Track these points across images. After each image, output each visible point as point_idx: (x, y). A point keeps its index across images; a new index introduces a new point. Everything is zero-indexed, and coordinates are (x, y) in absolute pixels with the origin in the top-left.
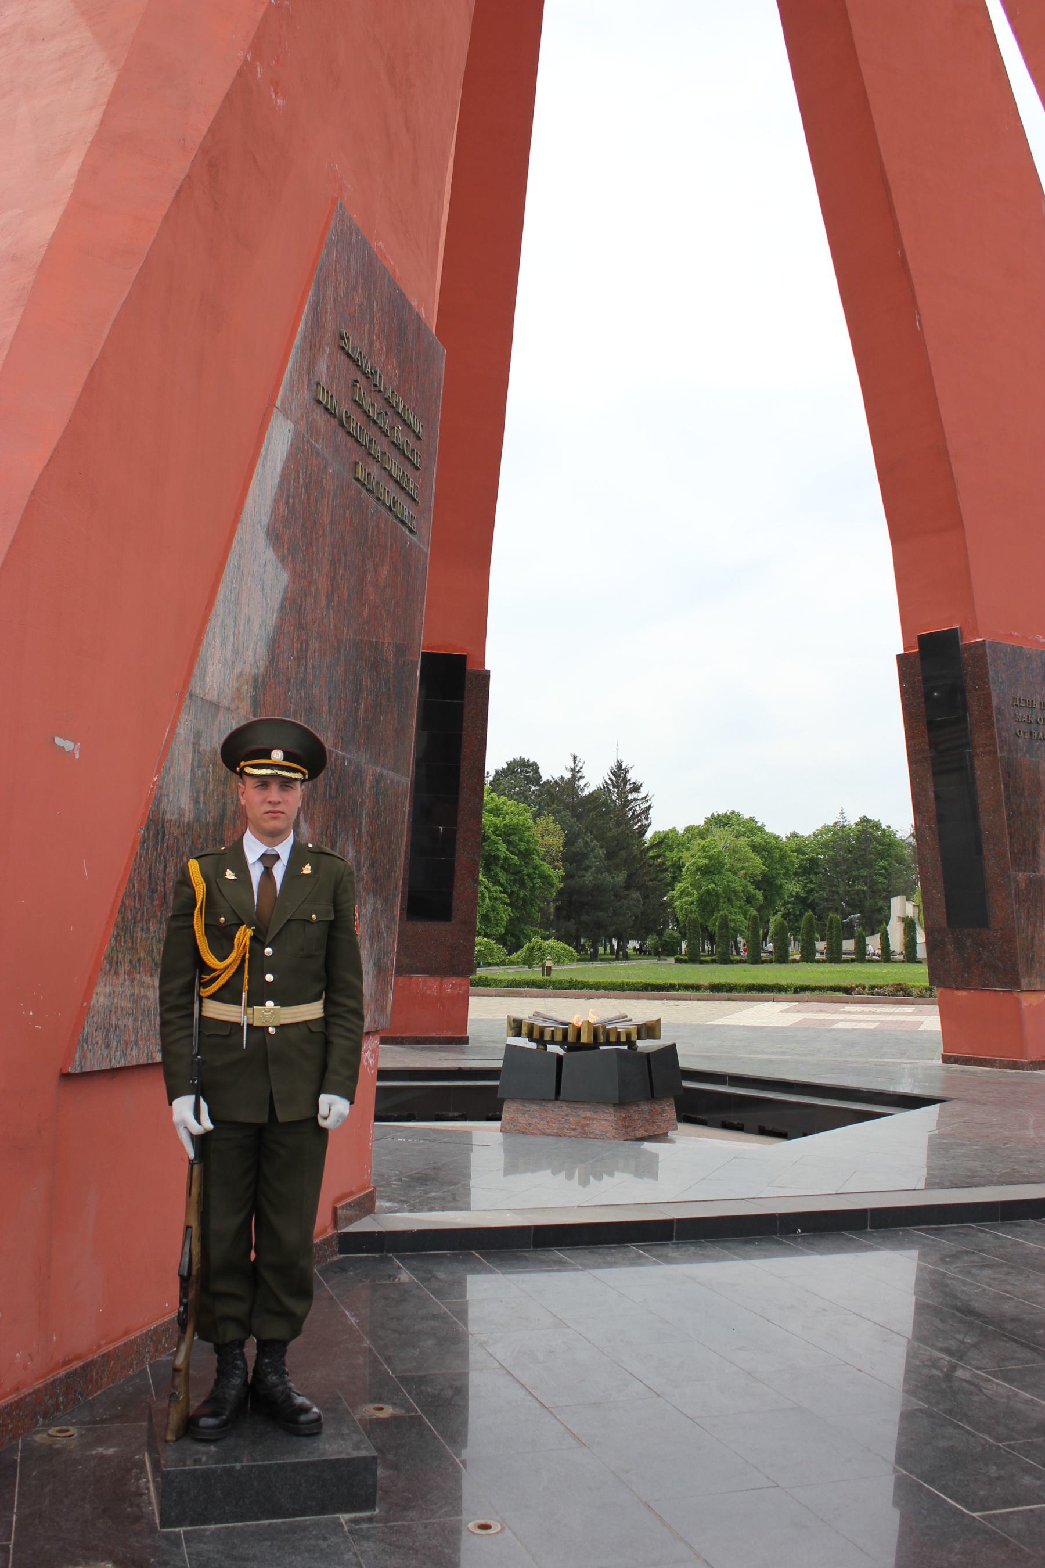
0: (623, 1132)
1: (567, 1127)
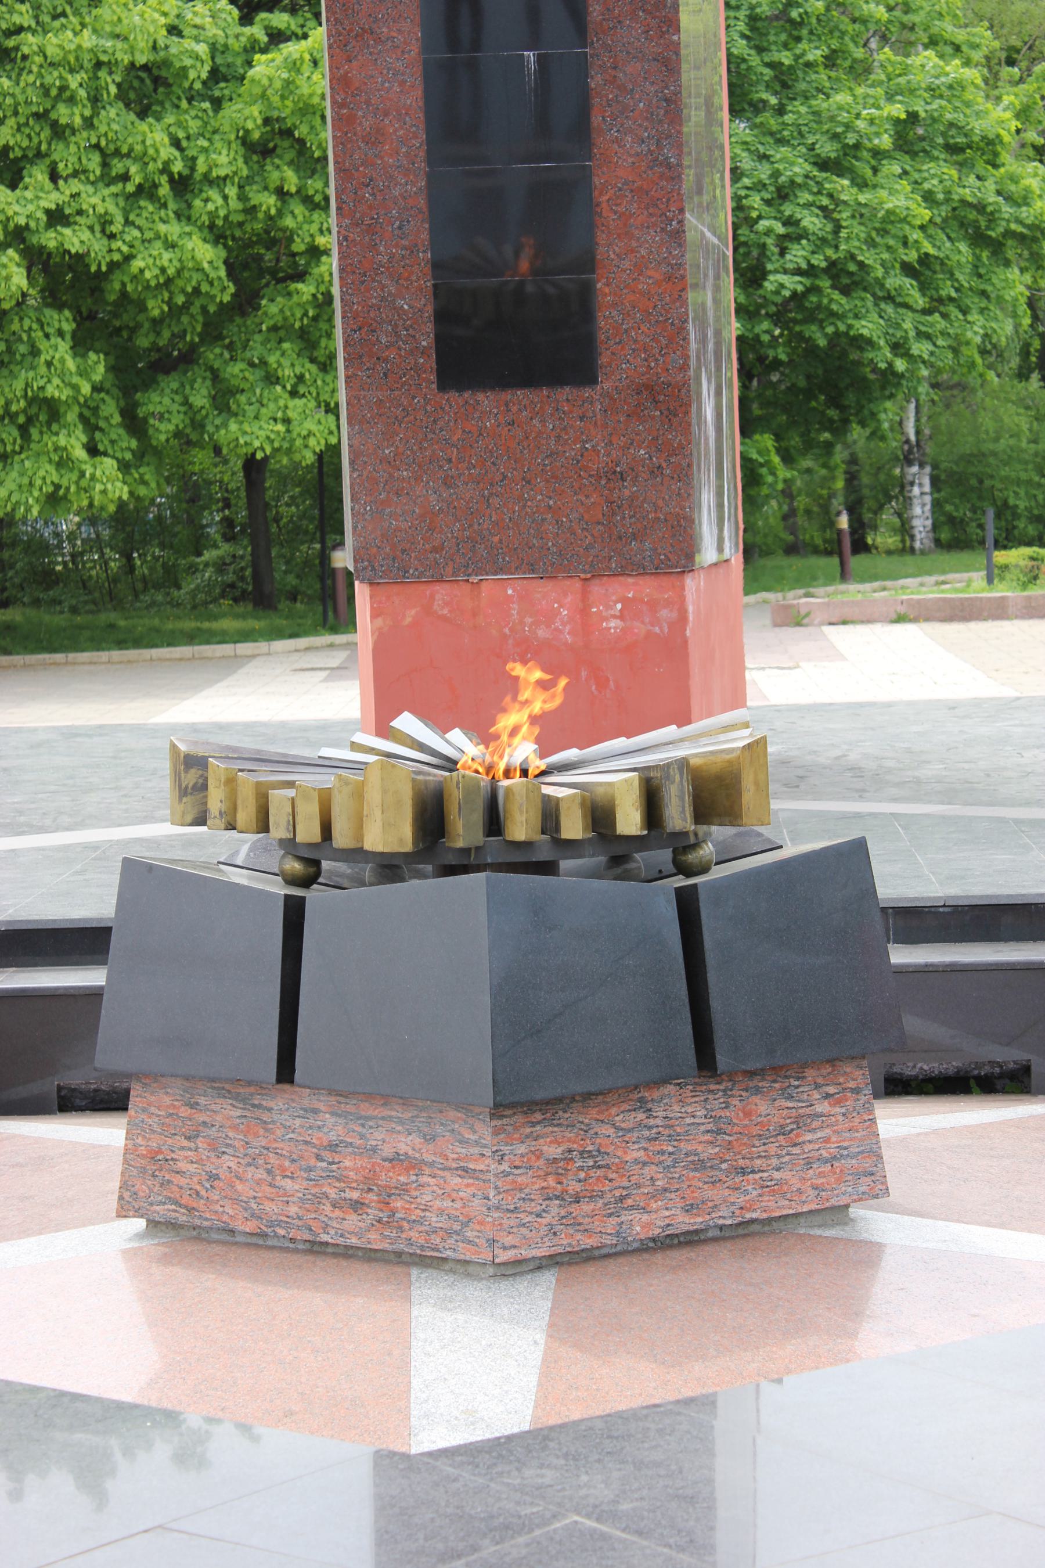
0: (547, 1219)
1: (332, 1193)
